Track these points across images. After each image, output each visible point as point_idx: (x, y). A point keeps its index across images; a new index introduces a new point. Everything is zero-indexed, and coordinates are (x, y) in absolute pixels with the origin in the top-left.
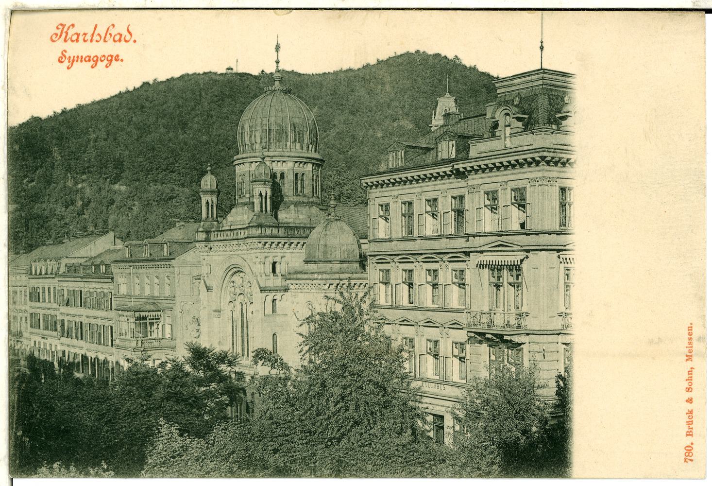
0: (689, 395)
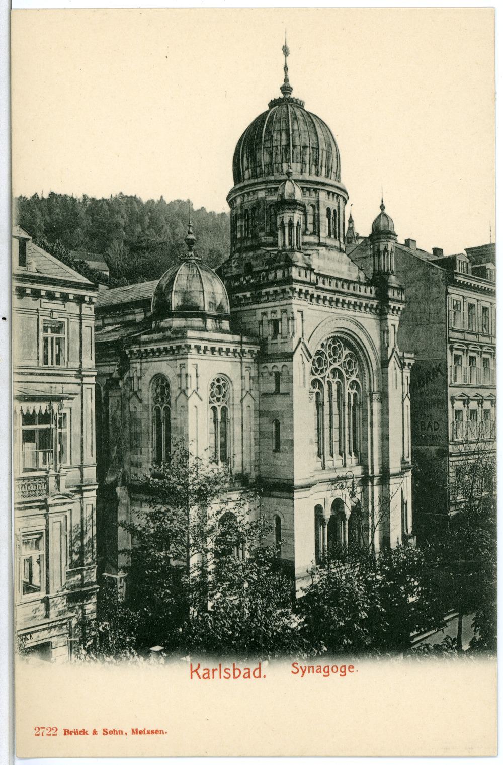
0: (100, 732)
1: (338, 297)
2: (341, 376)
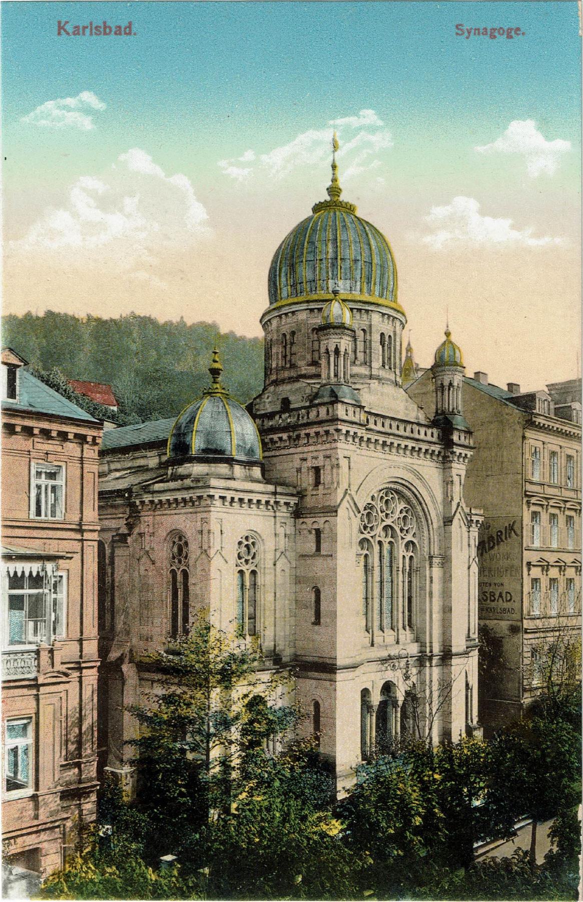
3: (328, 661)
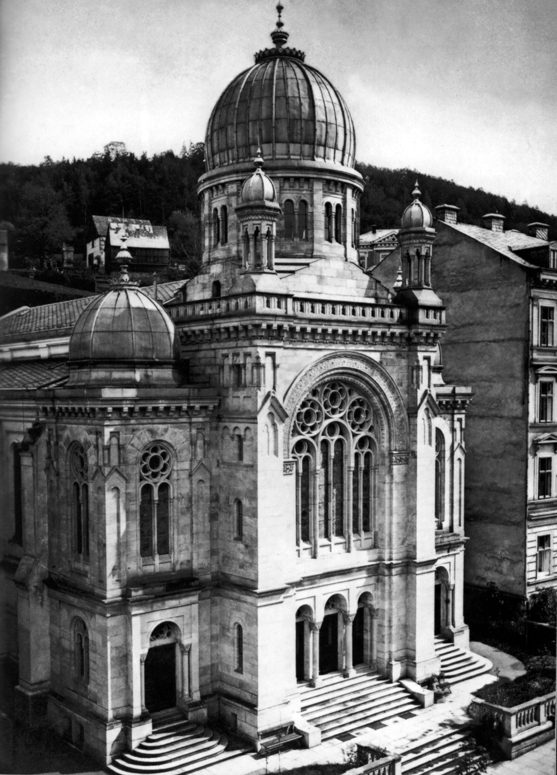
1: (335, 328)
2: (343, 431)
3: (249, 583)
